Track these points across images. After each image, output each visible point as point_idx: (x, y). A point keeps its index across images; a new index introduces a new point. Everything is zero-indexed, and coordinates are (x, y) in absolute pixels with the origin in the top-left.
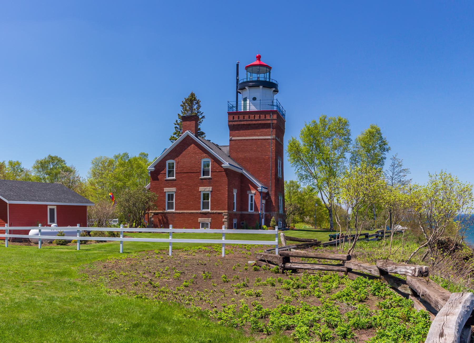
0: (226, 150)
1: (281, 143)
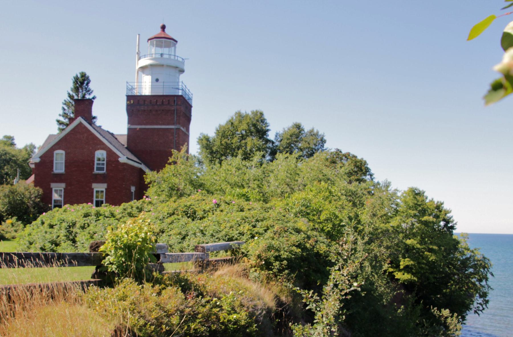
0: (124, 141)
1: (187, 133)
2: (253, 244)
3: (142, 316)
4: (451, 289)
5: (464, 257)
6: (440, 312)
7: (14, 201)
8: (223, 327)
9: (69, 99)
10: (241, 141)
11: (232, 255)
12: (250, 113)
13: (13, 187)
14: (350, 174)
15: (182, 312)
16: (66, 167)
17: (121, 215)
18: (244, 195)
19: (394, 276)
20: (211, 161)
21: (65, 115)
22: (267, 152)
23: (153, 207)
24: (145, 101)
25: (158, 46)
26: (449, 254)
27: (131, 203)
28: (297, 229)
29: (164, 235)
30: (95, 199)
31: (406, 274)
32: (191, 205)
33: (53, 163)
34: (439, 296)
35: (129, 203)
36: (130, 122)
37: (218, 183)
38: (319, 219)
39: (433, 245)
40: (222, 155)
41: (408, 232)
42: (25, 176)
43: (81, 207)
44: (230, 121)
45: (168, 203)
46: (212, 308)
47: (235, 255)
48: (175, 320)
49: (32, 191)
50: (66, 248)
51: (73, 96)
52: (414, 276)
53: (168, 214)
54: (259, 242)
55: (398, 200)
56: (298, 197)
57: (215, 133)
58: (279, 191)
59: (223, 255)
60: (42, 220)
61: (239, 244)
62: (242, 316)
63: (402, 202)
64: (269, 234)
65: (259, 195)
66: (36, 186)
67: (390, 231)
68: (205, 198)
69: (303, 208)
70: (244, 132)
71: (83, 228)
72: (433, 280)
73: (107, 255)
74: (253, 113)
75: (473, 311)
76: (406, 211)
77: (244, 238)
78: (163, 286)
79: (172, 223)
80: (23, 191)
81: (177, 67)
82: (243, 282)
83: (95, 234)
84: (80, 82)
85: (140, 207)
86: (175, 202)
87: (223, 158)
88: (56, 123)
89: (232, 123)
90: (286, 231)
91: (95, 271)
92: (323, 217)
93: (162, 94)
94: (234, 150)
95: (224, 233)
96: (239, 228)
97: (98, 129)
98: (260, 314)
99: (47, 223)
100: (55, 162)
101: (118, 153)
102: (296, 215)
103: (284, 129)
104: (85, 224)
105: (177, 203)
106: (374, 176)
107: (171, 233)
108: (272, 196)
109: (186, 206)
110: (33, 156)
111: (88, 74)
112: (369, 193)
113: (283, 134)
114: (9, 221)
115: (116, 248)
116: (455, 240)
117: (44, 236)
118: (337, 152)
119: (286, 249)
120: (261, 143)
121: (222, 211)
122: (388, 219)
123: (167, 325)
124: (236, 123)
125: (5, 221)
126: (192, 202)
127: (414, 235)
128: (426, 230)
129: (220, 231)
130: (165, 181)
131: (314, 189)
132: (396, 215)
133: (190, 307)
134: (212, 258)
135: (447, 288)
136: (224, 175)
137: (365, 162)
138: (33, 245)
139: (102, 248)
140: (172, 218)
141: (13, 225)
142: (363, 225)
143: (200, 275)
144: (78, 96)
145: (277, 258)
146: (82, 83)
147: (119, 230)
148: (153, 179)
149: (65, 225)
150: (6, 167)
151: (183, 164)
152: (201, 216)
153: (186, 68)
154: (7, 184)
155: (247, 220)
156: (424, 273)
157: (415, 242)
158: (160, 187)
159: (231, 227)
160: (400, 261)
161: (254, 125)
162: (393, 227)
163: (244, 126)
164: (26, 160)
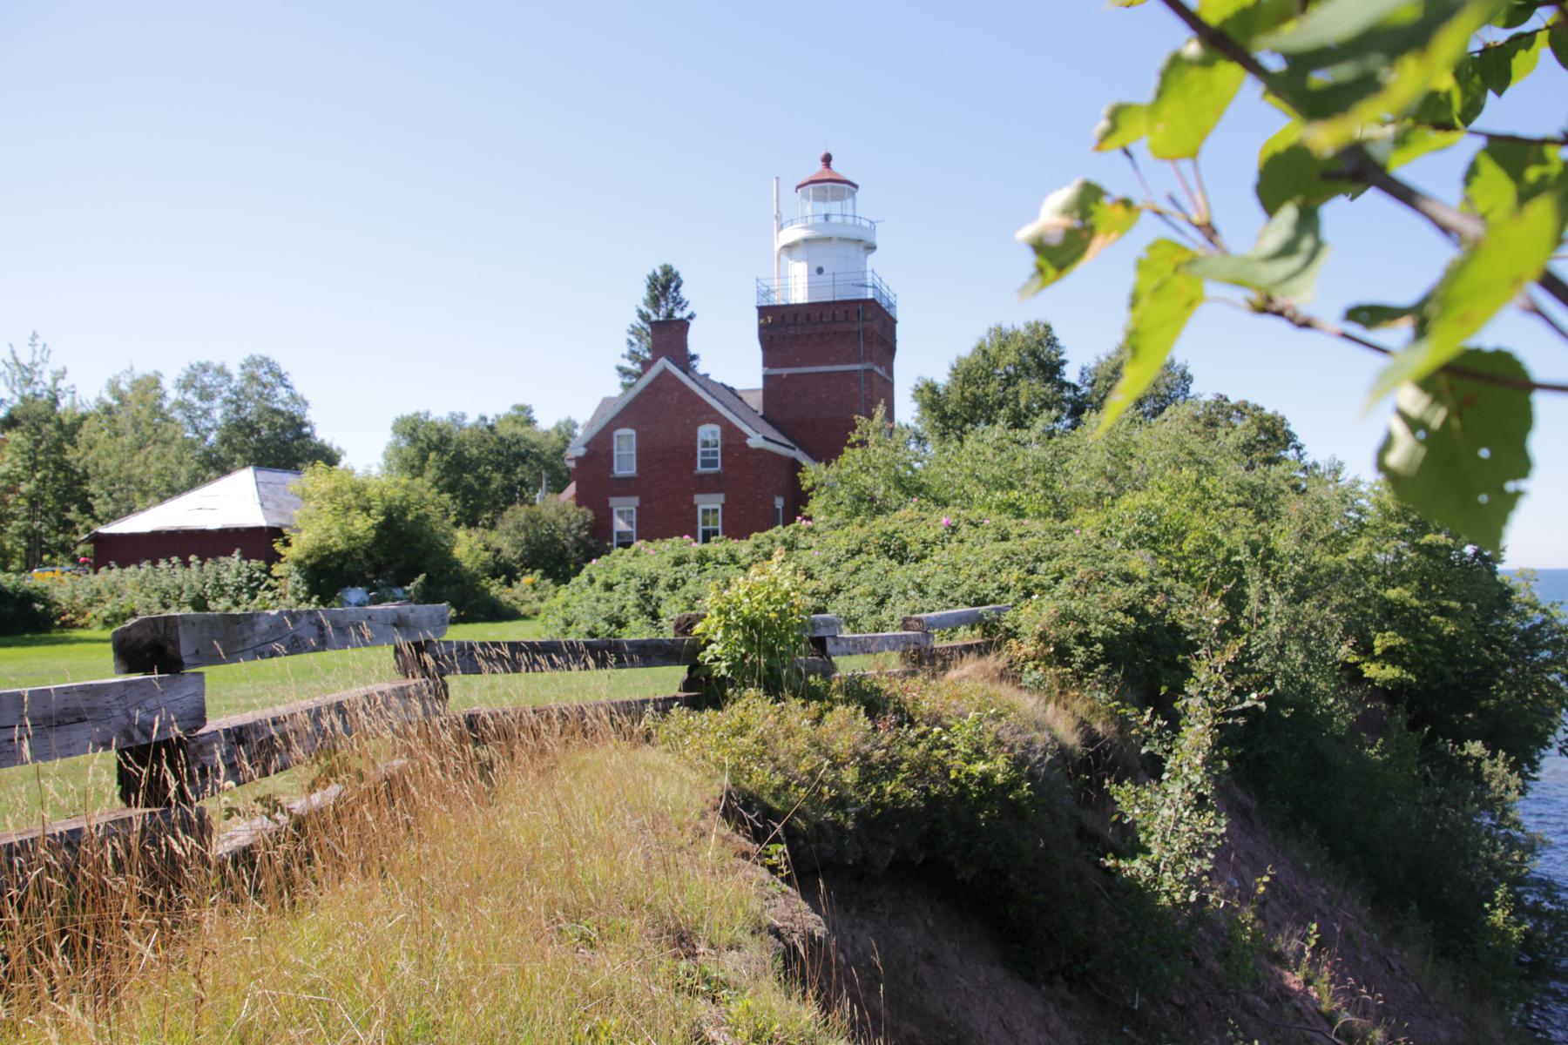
0: (756, 402)
2: (1029, 610)
3: (779, 768)
4: (1498, 698)
5: (1527, 626)
6: (1463, 748)
7: (537, 539)
8: (956, 790)
9: (640, 321)
10: (1005, 389)
11: (983, 636)
12: (1022, 328)
13: (534, 509)
14: (1248, 448)
15: (866, 757)
16: (639, 462)
17: (749, 559)
18: (1012, 505)
19: (1362, 672)
20: (943, 435)
21: (634, 356)
22: (1063, 409)
23: (817, 539)
24: (796, 316)
25: (820, 198)
26: (1489, 619)
27: (771, 532)
28: (1126, 574)
29: (841, 597)
30: (700, 528)
31: (1388, 667)
32: (895, 532)
33: (612, 457)
34: (1470, 715)
35: (767, 533)
36: (767, 362)
37: (958, 481)
38: (1181, 549)
39: (1450, 599)
40: (966, 421)
41: (1389, 573)
42: (558, 486)
43: (668, 546)
44: (980, 348)
45: (847, 529)
46: (931, 749)
47: (990, 635)
48: (850, 775)
49: (573, 516)
50: (638, 631)
51: (649, 316)
52: (1408, 672)
53: (847, 551)
54: (1042, 606)
55: (1363, 502)
56: (1131, 502)
57: (950, 375)
58: (1091, 491)
59: (965, 636)
60: (590, 575)
61: (999, 612)
62: (999, 767)
63: (1373, 504)
64: (1064, 586)
65: (1046, 503)
66: (579, 505)
67: (1347, 571)
68: (924, 515)
69: (1143, 527)
70: (1011, 370)
71: (673, 587)
72: (1453, 680)
73: (710, 642)
74: (1028, 327)
75: (1554, 751)
76: (1383, 526)
77: (1010, 598)
78: (827, 703)
79: (858, 569)
80: (554, 516)
81: (860, 241)
82: (1006, 691)
83: (697, 599)
84: (662, 286)
85: (789, 540)
86: (861, 526)
87: (968, 426)
88: (617, 372)
89: (985, 352)
90: (1103, 580)
91: (686, 676)
92: (1188, 547)
93: (831, 299)
94: (992, 409)
95: (965, 588)
96: (998, 576)
97: (702, 381)
98: (1041, 760)
99: (600, 580)
100: (616, 453)
101: (746, 429)
102: (1127, 544)
103: (1098, 358)
104: (676, 580)
105: (866, 528)
106: (1305, 449)
107: (854, 592)
108: (1076, 504)
109: (885, 534)
110: (573, 443)
111: (676, 269)
112: (1295, 487)
113: (1096, 369)
114: (527, 580)
115: (727, 628)
116: (1502, 585)
117: (594, 608)
118: (1217, 402)
119: (1101, 617)
120: (1048, 389)
121: (961, 541)
122: (1342, 544)
123: (832, 785)
124: (993, 351)
125: (518, 580)
126: (899, 524)
127: (1404, 580)
128: (1431, 565)
129: (958, 585)
130: (843, 483)
131: (1165, 484)
132: (1359, 536)
133: (883, 747)
134: (939, 643)
135: (1488, 694)
136: (969, 463)
137: (1283, 419)
138: (573, 626)
139: (699, 628)
140: (857, 560)
141: (534, 587)
142: (1280, 560)
143: (910, 682)
144: (658, 314)
145: (1083, 639)
146: (666, 287)
147: (734, 588)
148: (818, 479)
149: (635, 582)
150: (519, 470)
151: (880, 446)
152: (917, 553)
153: (878, 241)
154: (521, 504)
155: (1015, 558)
156: (1432, 664)
157: (1407, 594)
158: (833, 497)
159: (982, 575)
160: (1373, 640)
161: (1033, 353)
162: (1354, 562)
163: (1011, 357)
164: (560, 453)
